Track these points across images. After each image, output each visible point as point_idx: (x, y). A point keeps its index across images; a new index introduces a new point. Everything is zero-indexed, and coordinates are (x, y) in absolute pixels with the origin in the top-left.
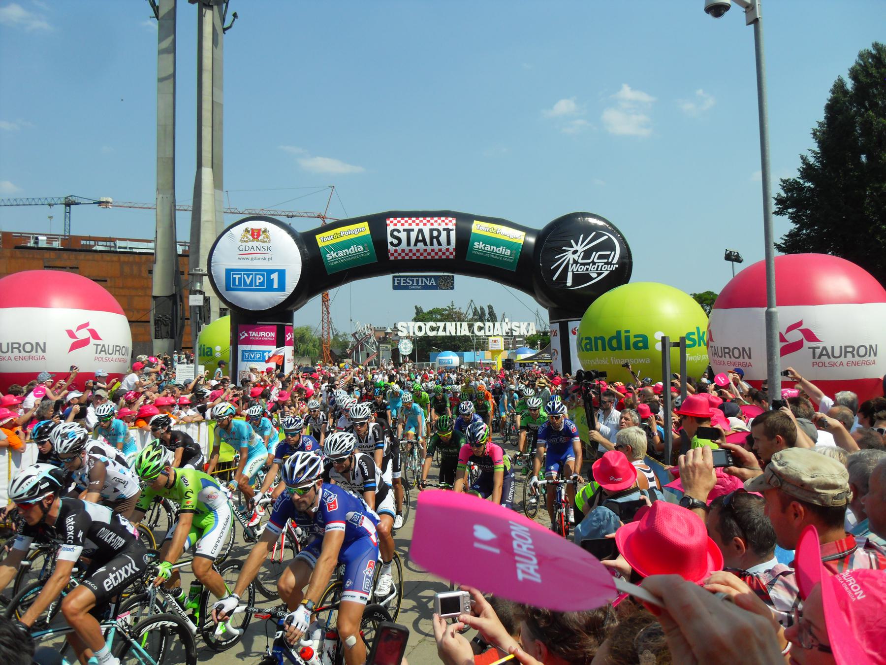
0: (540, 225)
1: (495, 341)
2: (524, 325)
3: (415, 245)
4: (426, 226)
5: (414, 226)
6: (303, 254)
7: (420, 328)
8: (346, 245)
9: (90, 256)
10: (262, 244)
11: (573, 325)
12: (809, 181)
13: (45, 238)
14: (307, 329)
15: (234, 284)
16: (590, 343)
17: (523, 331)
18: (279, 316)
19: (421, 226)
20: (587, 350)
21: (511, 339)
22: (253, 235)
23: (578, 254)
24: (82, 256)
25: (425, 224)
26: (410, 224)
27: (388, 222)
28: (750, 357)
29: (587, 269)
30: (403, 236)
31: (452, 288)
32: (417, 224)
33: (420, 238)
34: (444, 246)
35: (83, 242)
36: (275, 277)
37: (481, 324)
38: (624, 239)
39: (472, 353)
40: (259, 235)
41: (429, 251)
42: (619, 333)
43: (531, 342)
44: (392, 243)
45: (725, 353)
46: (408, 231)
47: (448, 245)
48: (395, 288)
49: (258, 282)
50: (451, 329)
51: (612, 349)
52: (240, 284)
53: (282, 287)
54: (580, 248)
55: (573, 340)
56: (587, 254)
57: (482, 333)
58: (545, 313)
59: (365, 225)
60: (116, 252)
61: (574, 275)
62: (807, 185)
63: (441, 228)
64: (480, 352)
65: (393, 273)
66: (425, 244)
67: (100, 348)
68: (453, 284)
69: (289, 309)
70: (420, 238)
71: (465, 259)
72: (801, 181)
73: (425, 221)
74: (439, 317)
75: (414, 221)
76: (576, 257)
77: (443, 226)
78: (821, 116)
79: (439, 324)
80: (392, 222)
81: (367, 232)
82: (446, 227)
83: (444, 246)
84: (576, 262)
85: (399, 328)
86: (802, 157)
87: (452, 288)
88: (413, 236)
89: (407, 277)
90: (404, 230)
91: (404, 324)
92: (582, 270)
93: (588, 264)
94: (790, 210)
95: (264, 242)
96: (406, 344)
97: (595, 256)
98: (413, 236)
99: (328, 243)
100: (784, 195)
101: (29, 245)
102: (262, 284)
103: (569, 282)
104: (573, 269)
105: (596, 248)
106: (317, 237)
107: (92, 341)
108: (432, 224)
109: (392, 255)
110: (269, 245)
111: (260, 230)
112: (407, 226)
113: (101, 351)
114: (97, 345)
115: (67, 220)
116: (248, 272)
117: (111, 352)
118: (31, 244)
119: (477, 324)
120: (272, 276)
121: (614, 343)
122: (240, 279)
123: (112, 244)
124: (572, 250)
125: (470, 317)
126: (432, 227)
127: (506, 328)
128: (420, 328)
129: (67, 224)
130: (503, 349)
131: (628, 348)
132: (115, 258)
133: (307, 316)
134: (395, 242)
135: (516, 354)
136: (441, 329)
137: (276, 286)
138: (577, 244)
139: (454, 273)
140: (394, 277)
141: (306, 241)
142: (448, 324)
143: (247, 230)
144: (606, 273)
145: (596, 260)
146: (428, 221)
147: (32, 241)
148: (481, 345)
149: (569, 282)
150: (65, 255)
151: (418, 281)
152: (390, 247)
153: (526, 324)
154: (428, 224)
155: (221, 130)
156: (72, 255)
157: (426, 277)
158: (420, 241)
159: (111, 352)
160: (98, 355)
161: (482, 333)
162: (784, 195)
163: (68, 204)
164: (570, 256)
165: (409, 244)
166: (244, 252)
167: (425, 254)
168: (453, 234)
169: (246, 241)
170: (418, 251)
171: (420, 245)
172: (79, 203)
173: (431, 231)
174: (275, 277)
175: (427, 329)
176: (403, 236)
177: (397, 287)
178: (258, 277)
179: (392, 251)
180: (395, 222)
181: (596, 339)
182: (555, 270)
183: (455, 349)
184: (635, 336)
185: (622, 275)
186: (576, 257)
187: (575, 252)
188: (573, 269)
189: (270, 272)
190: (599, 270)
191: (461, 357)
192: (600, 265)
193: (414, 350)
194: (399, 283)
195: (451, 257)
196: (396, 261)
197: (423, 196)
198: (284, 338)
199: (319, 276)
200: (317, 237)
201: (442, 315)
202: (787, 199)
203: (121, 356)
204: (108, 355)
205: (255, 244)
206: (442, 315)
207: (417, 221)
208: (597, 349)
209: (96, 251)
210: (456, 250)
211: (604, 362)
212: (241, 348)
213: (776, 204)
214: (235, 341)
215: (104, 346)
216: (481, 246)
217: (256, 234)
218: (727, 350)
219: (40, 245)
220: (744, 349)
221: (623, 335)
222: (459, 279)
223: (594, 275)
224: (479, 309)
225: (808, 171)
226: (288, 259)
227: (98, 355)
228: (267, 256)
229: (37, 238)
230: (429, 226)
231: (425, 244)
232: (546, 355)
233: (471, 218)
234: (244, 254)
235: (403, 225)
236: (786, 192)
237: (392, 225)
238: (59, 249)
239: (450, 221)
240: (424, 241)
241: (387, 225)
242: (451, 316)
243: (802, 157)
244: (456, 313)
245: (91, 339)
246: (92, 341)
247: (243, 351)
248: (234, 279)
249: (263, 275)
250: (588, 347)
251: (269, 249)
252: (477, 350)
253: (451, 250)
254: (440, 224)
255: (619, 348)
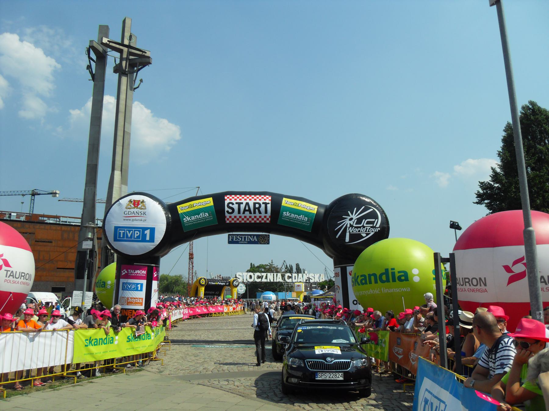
0: (328, 201)
1: (299, 286)
2: (317, 276)
3: (244, 213)
4: (251, 201)
5: (243, 201)
6: (167, 218)
7: (251, 277)
8: (197, 212)
9: (43, 226)
10: (140, 210)
11: (349, 269)
12: (497, 183)
13: (15, 214)
14: (179, 277)
15: (120, 237)
16: (365, 279)
17: (317, 280)
18: (151, 259)
19: (248, 201)
20: (363, 284)
21: (309, 285)
22: (134, 204)
23: (353, 220)
24: (38, 226)
25: (250, 200)
26: (240, 200)
27: (226, 198)
28: (485, 285)
29: (359, 231)
30: (236, 207)
31: (268, 243)
32: (245, 200)
33: (247, 208)
34: (263, 215)
35: (40, 218)
36: (148, 232)
37: (290, 275)
38: (383, 211)
39: (284, 293)
40: (138, 204)
41: (253, 217)
42: (387, 270)
43: (322, 286)
44: (228, 212)
45: (466, 282)
46: (239, 204)
47: (266, 216)
48: (230, 242)
49: (136, 235)
50: (270, 277)
51: (382, 281)
52: (124, 237)
53: (152, 239)
54: (355, 217)
55: (349, 278)
56: (359, 221)
57: (290, 280)
58: (329, 262)
59: (211, 199)
60: (59, 224)
61: (350, 234)
62: (496, 185)
63: (261, 202)
64: (289, 293)
65: (229, 232)
66: (250, 213)
67: (9, 273)
68: (269, 241)
69: (157, 255)
70: (247, 208)
71: (278, 222)
72: (492, 183)
73: (250, 198)
74: (263, 270)
75: (243, 198)
76: (351, 222)
77: (263, 201)
78: (501, 144)
79: (263, 274)
80: (228, 198)
81: (212, 204)
82: (265, 201)
83: (263, 215)
84: (351, 226)
85: (238, 276)
86: (492, 168)
87: (268, 243)
88: (242, 207)
89: (238, 235)
90: (236, 203)
91: (241, 274)
92: (356, 231)
93: (360, 227)
94: (486, 201)
95: (141, 209)
96: (241, 287)
97: (364, 222)
98: (242, 207)
99: (185, 211)
100: (481, 192)
101: (5, 218)
102: (138, 237)
103: (347, 239)
104: (350, 230)
105: (365, 217)
106: (178, 207)
107: (4, 268)
108: (255, 200)
109: (228, 219)
110: (145, 211)
111: (139, 201)
112: (238, 201)
113: (10, 275)
114: (7, 271)
115: (32, 204)
116: (130, 228)
117: (17, 276)
118: (6, 217)
119: (287, 275)
120: (146, 232)
121: (384, 278)
122: (124, 233)
123: (58, 220)
124: (349, 218)
125: (283, 270)
126: (255, 202)
127: (305, 277)
128: (251, 277)
129: (32, 207)
130: (304, 291)
131: (394, 280)
132: (59, 228)
133: (173, 263)
134: (230, 211)
135: (312, 294)
136: (264, 277)
137: (148, 238)
138: (352, 214)
139: (269, 233)
140: (229, 235)
141: (171, 210)
142: (269, 274)
143: (130, 201)
144: (372, 234)
145: (365, 225)
146: (253, 198)
147: (7, 216)
148: (290, 288)
149: (347, 239)
150: (27, 225)
151: (245, 238)
152: (226, 214)
153: (318, 275)
154: (253, 200)
155: (129, 148)
156: (32, 225)
157: (250, 235)
158: (247, 211)
159: (17, 276)
160: (7, 278)
161: (290, 280)
162: (481, 192)
163: (34, 194)
164: (348, 222)
165: (239, 212)
166: (128, 215)
167: (250, 219)
168: (269, 206)
169: (130, 208)
170: (245, 217)
171: (247, 213)
172: (39, 194)
173: (255, 204)
174: (148, 232)
175: (255, 278)
176: (236, 207)
177: (231, 242)
178: (136, 232)
179: (228, 217)
180: (231, 198)
181: (370, 275)
182: (339, 228)
183: (274, 291)
184: (399, 272)
185: (383, 233)
186: (351, 222)
187: (351, 219)
188: (350, 230)
189: (145, 229)
190: (367, 231)
191: (277, 295)
192: (368, 228)
193: (246, 291)
194: (232, 239)
195: (268, 222)
196: (230, 223)
197: (249, 176)
198: (153, 275)
199: (179, 231)
200: (178, 207)
201: (265, 269)
202: (484, 194)
203: (25, 281)
204: (15, 279)
205: (135, 210)
206: (265, 269)
207: (245, 198)
208: (370, 283)
209: (47, 223)
210: (271, 217)
211: (377, 292)
212: (122, 281)
213: (477, 197)
214: (119, 276)
215: (12, 272)
216: (288, 214)
217: (136, 204)
218: (467, 280)
219: (12, 219)
220: (480, 279)
221: (390, 271)
222: (274, 238)
223: (364, 235)
224: (288, 266)
225: (496, 177)
226: (157, 219)
227: (7, 278)
228: (143, 219)
229: (10, 214)
230: (253, 201)
231: (250, 213)
232: (332, 293)
233: (282, 196)
234: (127, 217)
235: (236, 200)
236: (483, 189)
237: (228, 200)
238: (24, 222)
239: (268, 198)
240: (249, 210)
241: (225, 200)
242: (270, 269)
243: (492, 168)
244: (274, 267)
245: (3, 266)
246: (4, 268)
247: (123, 283)
248: (120, 233)
249: (140, 231)
250: (363, 281)
251: (144, 213)
252: (287, 291)
253: (268, 217)
254: (261, 200)
255: (388, 280)
